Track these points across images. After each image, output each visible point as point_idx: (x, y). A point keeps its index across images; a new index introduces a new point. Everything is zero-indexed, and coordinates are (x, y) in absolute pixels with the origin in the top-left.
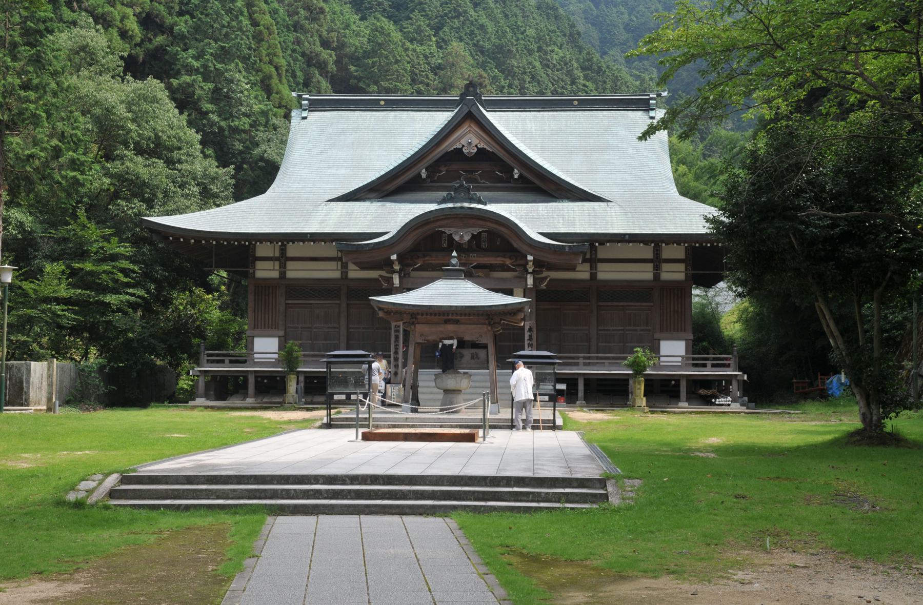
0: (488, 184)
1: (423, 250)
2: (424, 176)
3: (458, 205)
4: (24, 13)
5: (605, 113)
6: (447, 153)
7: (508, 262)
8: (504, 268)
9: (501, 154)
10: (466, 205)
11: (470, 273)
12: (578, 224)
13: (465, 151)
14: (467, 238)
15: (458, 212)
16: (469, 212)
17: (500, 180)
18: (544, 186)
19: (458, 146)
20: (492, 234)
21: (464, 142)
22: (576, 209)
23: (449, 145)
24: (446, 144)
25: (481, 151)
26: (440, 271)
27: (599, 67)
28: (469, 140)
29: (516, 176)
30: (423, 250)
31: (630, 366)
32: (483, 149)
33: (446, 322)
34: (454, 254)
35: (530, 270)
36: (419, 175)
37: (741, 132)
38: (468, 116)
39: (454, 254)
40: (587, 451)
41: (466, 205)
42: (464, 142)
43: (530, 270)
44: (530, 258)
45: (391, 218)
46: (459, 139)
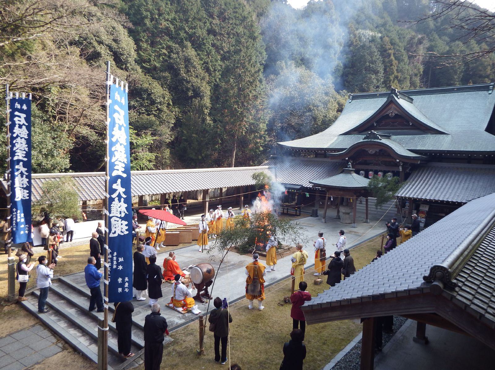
2: (375, 125)
3: (369, 140)
14: (374, 152)
24: (383, 113)
28: (392, 112)
41: (372, 140)
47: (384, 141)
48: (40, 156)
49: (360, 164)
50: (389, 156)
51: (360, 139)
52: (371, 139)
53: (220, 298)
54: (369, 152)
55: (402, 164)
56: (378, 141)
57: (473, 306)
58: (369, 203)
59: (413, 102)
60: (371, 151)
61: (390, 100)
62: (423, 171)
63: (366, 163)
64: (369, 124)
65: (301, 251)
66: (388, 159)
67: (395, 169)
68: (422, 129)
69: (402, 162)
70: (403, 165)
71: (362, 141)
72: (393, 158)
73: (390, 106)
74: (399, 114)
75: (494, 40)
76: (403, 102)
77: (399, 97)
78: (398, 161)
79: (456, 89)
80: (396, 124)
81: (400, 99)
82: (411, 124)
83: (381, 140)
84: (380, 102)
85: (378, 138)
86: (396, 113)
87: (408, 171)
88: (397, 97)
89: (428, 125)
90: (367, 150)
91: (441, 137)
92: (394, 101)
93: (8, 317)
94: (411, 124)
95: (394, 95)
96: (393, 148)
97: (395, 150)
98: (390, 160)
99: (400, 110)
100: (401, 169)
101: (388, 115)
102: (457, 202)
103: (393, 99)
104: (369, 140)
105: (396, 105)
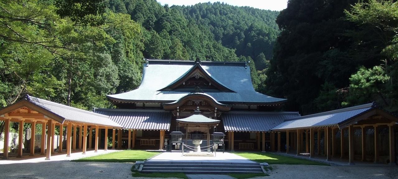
1: (187, 107)
2: (184, 84)
5: (233, 67)
6: (191, 78)
7: (209, 109)
8: (208, 111)
10: (199, 93)
11: (202, 112)
12: (228, 99)
19: (194, 76)
20: (206, 101)
21: (196, 75)
22: (227, 94)
24: (190, 76)
25: (200, 77)
26: (193, 112)
27: (218, 48)
28: (197, 74)
29: (210, 85)
30: (187, 107)
31: (370, 80)
33: (196, 126)
34: (198, 107)
35: (216, 112)
39: (198, 107)
41: (199, 93)
42: (196, 75)
43: (216, 112)
44: (216, 108)
45: (176, 97)
46: (195, 74)
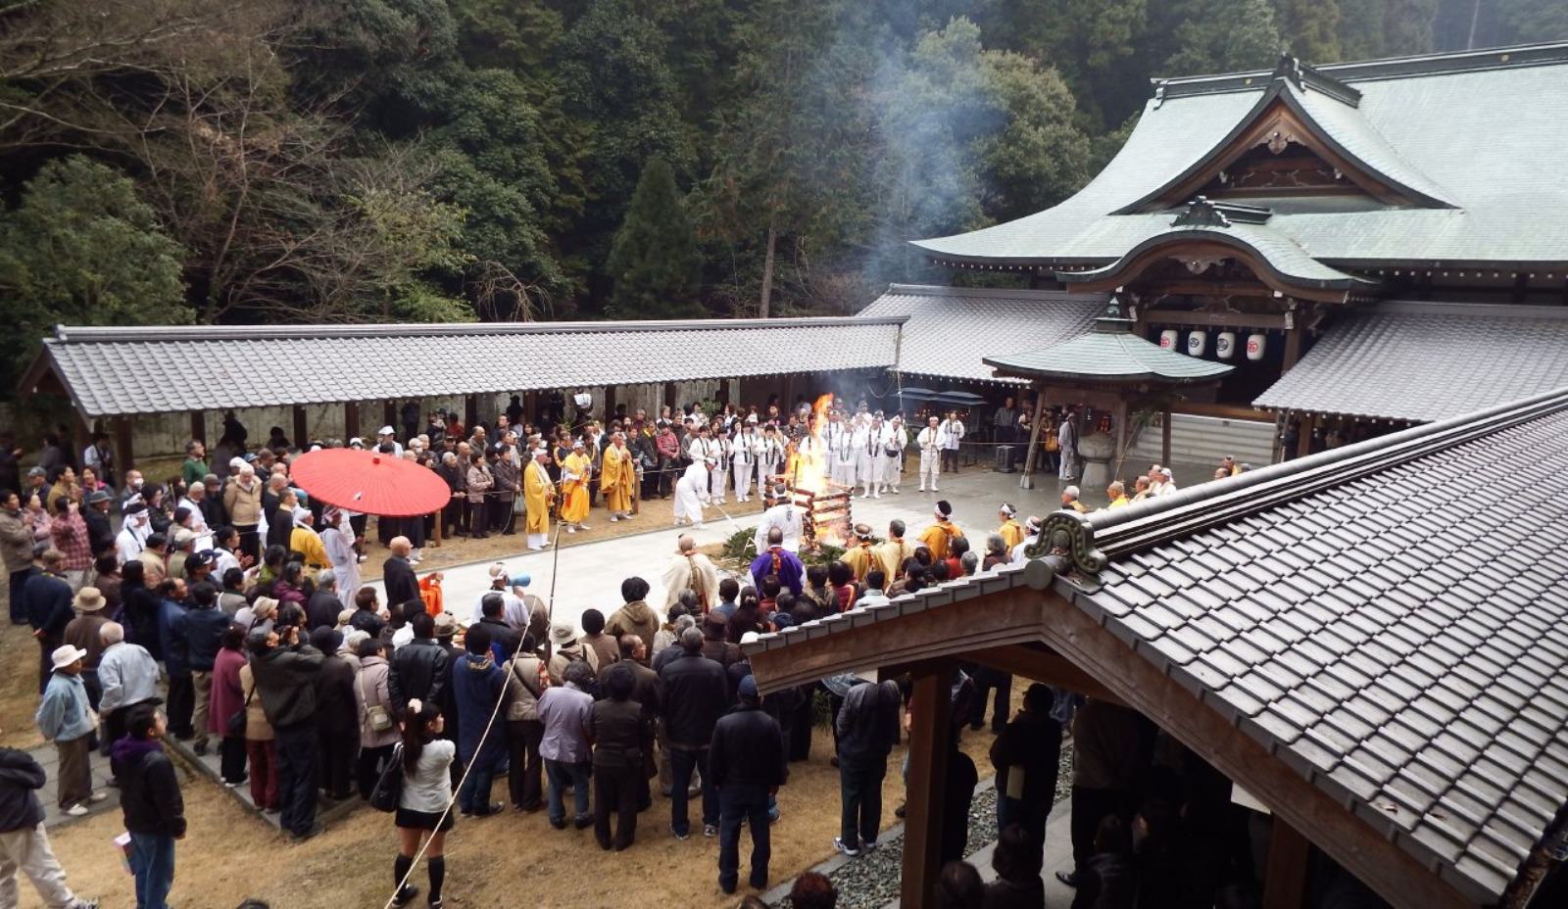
0: (1307, 186)
2: (1224, 180)
3: (1191, 227)
4: (610, 24)
9: (1316, 146)
13: (1272, 146)
14: (1204, 267)
15: (1191, 236)
16: (1203, 236)
17: (1323, 180)
18: (1373, 190)
19: (1263, 140)
23: (1251, 142)
24: (1250, 139)
25: (1292, 145)
28: (1280, 133)
32: (1295, 143)
36: (1218, 177)
37: (980, 146)
38: (1276, 103)
40: (834, 754)
41: (1201, 228)
47: (1239, 231)
48: (427, 575)
49: (1161, 306)
50: (1253, 279)
51: (1160, 224)
52: (1197, 223)
53: (648, 596)
54: (1191, 268)
55: (1293, 307)
56: (1220, 230)
57: (1467, 868)
58: (1173, 441)
59: (1362, 102)
60: (1197, 264)
61: (1273, 94)
62: (1362, 328)
63: (1187, 304)
64: (1204, 179)
65: (900, 542)
66: (1251, 292)
67: (1270, 323)
68: (1373, 190)
69: (1295, 299)
70: (1298, 309)
71: (1169, 230)
72: (1266, 287)
73: (1274, 116)
74: (1300, 141)
75: (630, 5)
76: (1319, 107)
77: (1303, 84)
78: (1278, 294)
79: (1505, 58)
80: (1292, 175)
81: (1308, 91)
82: (1338, 176)
83: (1228, 226)
84: (1245, 102)
85: (1219, 223)
86: (1293, 138)
87: (1312, 327)
88: (1298, 86)
89: (1393, 177)
90: (1182, 259)
91: (1442, 212)
92: (1286, 100)
93: (207, 795)
94: (1338, 176)
95: (1285, 79)
96: (1265, 254)
97: (1269, 259)
98: (1259, 292)
99: (1303, 131)
100: (1289, 323)
101: (1265, 146)
102: (1376, 418)
103: (1283, 94)
104: (1191, 227)
105: (1294, 116)
